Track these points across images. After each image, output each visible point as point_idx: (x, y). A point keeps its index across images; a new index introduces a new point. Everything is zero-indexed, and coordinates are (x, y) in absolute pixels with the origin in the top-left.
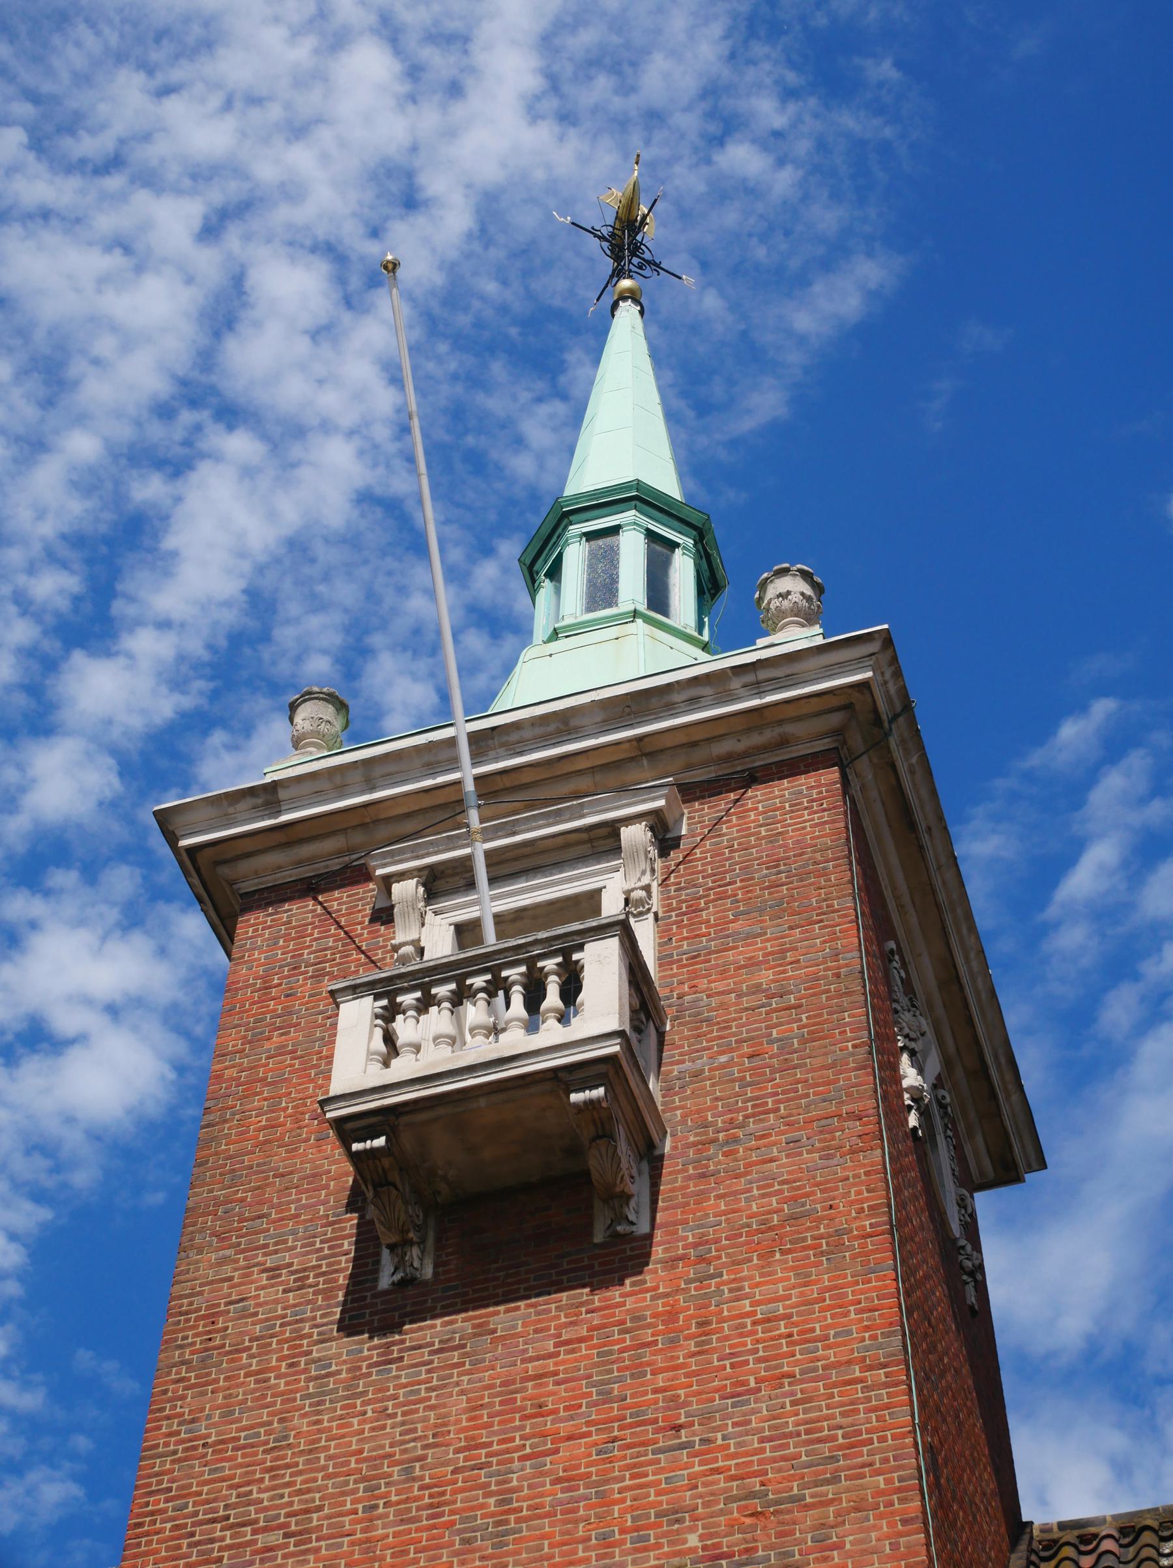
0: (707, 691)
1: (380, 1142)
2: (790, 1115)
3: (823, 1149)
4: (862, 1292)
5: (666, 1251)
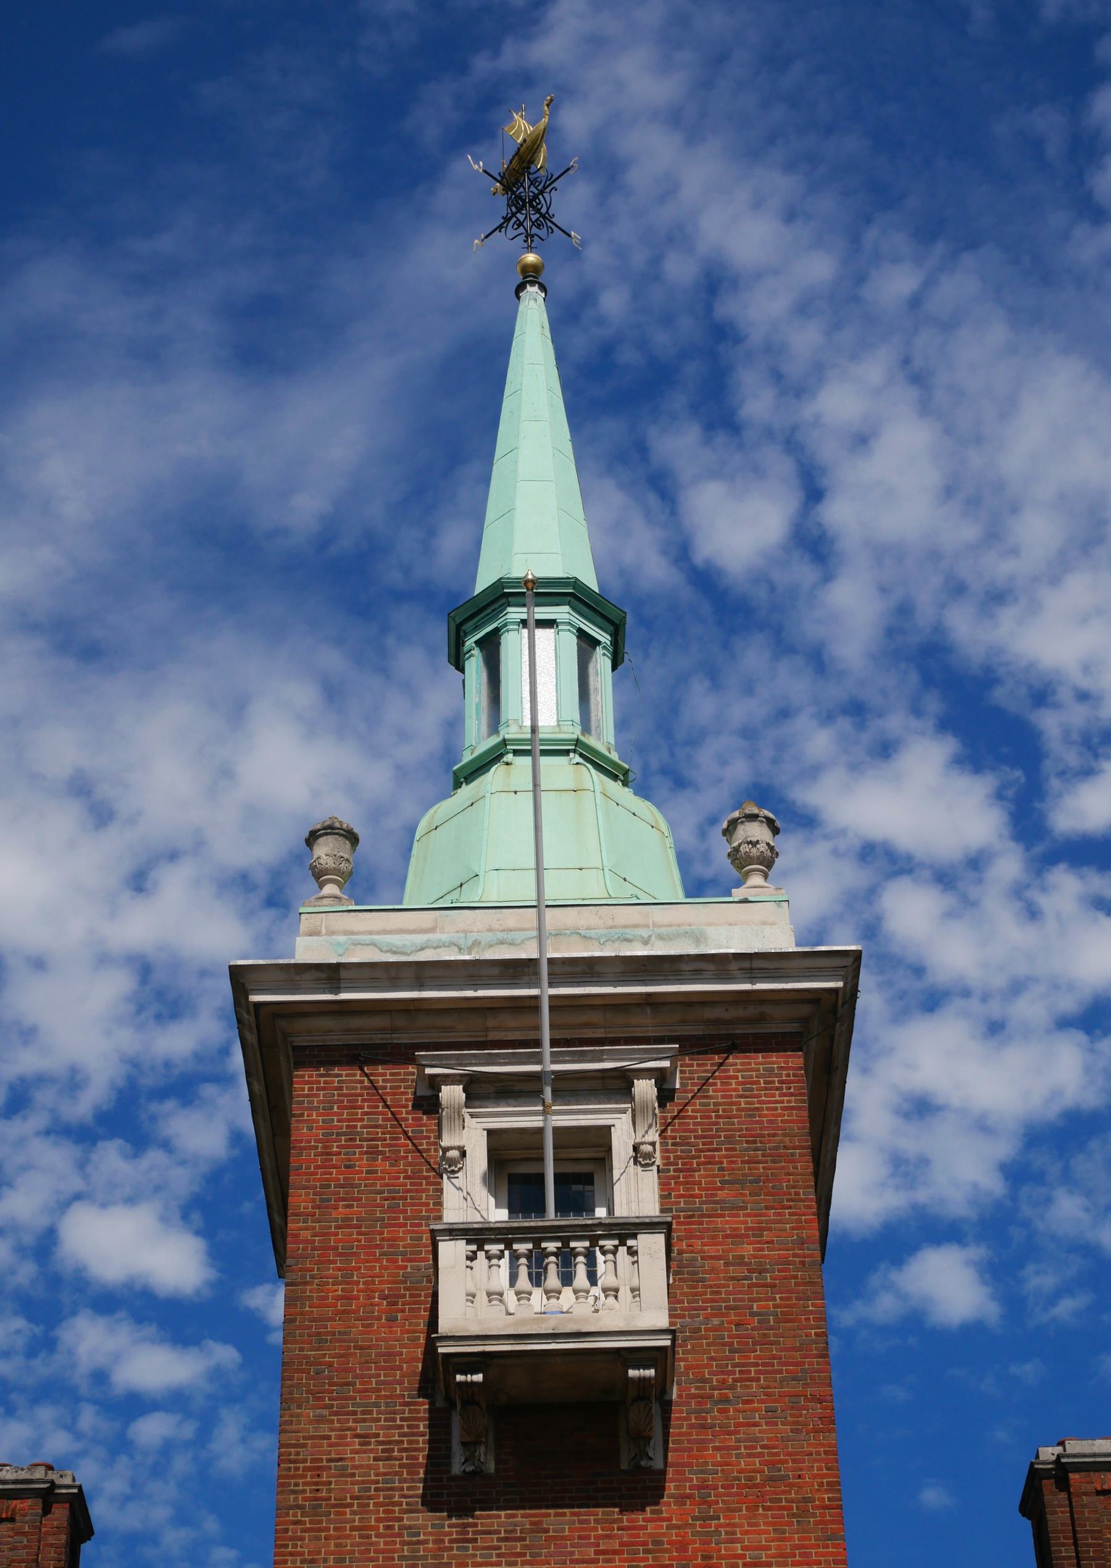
0: (710, 966)
1: (478, 1378)
2: (768, 1387)
3: (794, 1423)
4: (823, 1555)
5: (676, 1487)
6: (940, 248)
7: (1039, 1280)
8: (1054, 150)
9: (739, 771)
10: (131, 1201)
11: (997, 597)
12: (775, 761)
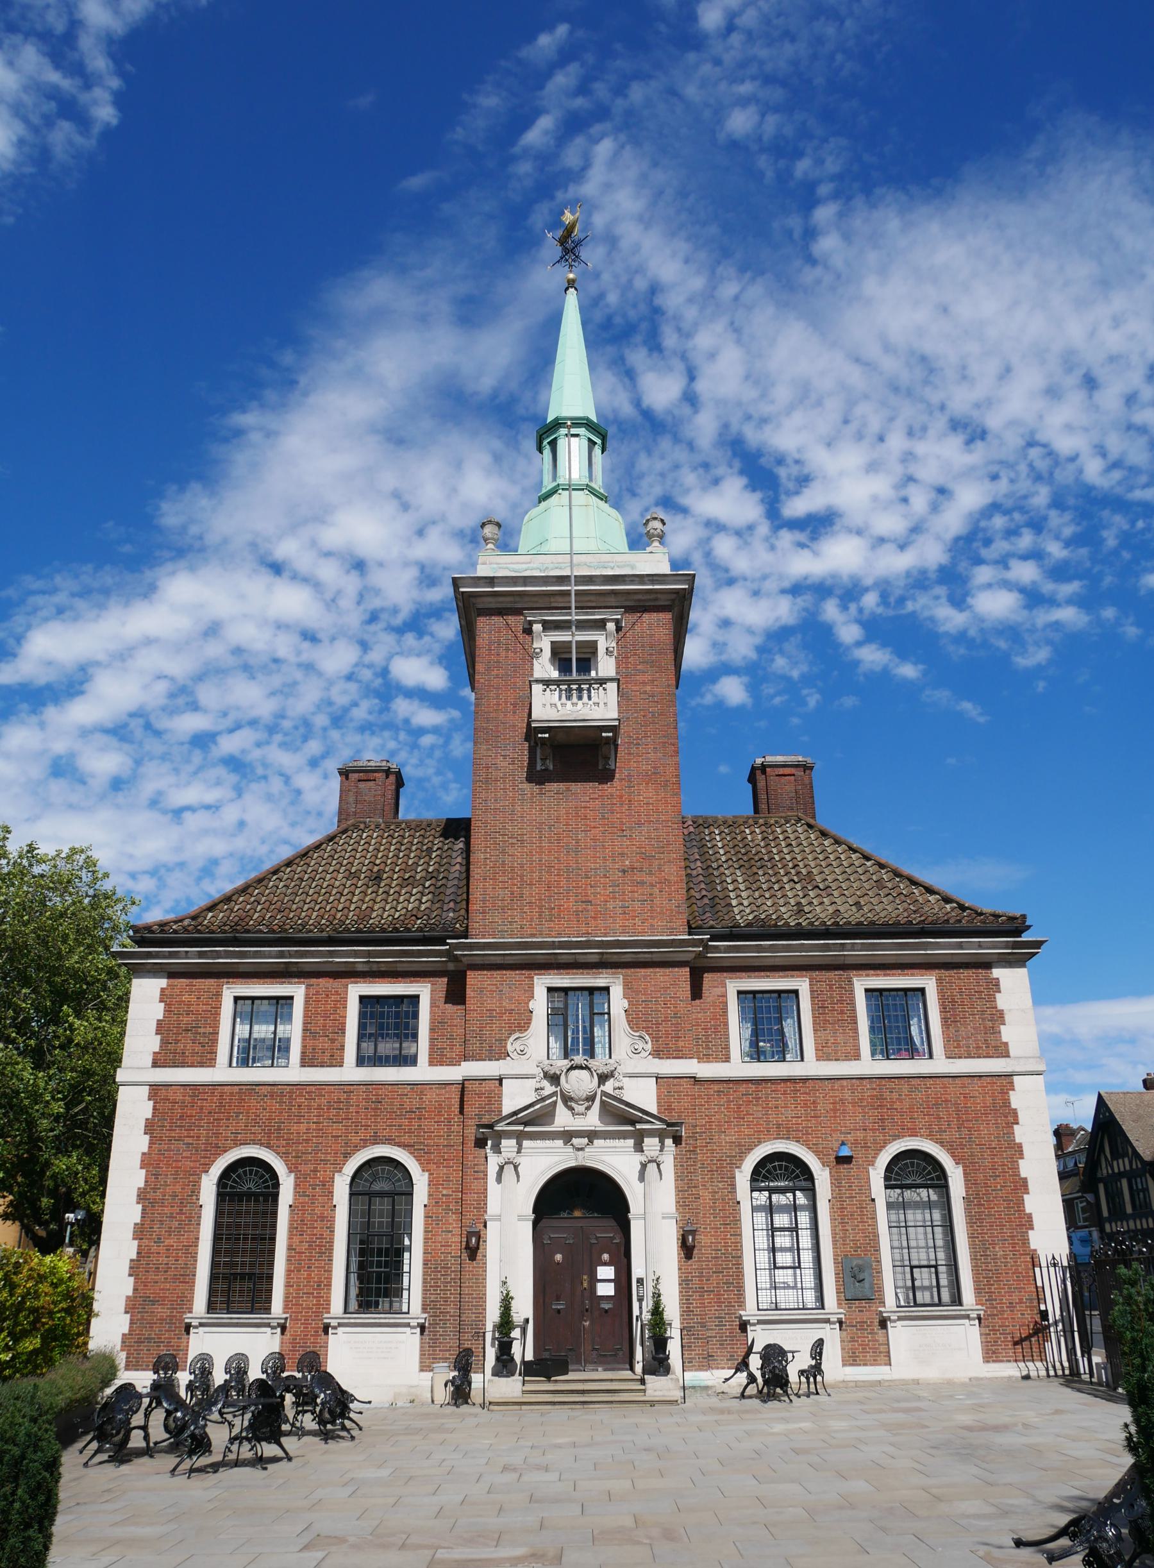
6: (748, 275)
7: (768, 689)
8: (797, 234)
9: (658, 491)
10: (419, 655)
11: (764, 421)
12: (673, 486)
